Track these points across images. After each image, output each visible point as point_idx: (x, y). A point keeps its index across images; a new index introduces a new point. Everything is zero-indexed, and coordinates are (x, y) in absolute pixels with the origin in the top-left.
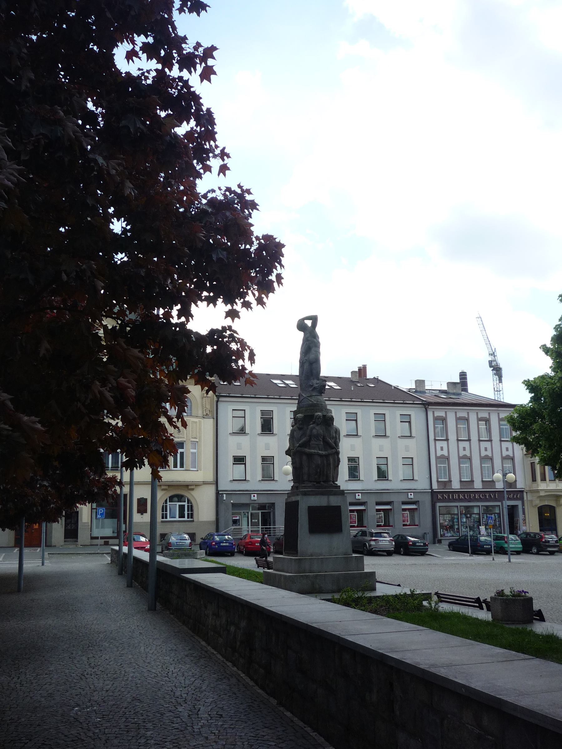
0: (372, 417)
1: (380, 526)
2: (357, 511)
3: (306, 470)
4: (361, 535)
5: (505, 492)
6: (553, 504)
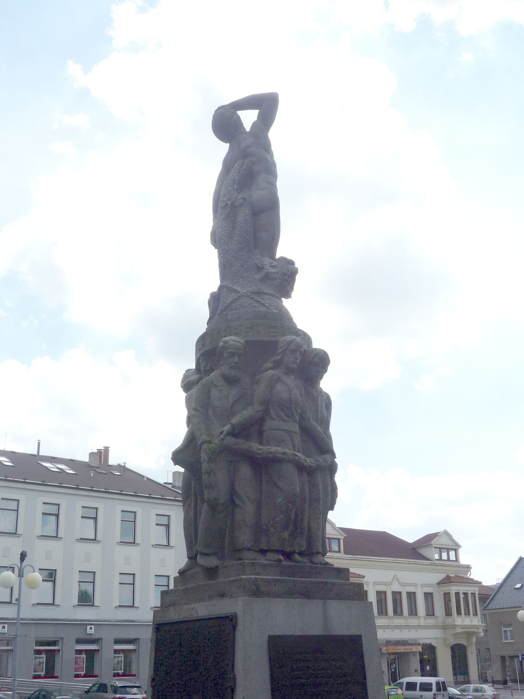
0: (119, 517)
1: (118, 675)
2: (87, 651)
3: (247, 512)
4: (98, 691)
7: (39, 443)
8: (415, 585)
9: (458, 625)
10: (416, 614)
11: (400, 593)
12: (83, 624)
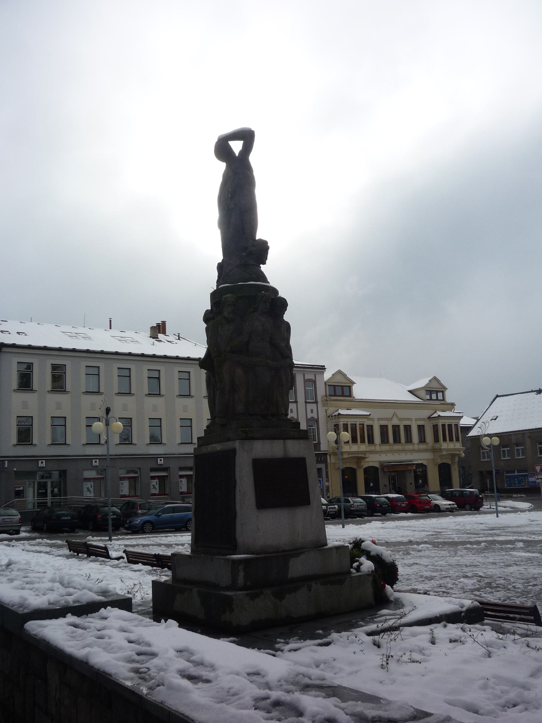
0: (176, 375)
5: (108, 460)
6: (354, 466)
7: (110, 321)
8: (410, 419)
9: (445, 449)
10: (411, 442)
11: (399, 426)
12: (155, 457)
